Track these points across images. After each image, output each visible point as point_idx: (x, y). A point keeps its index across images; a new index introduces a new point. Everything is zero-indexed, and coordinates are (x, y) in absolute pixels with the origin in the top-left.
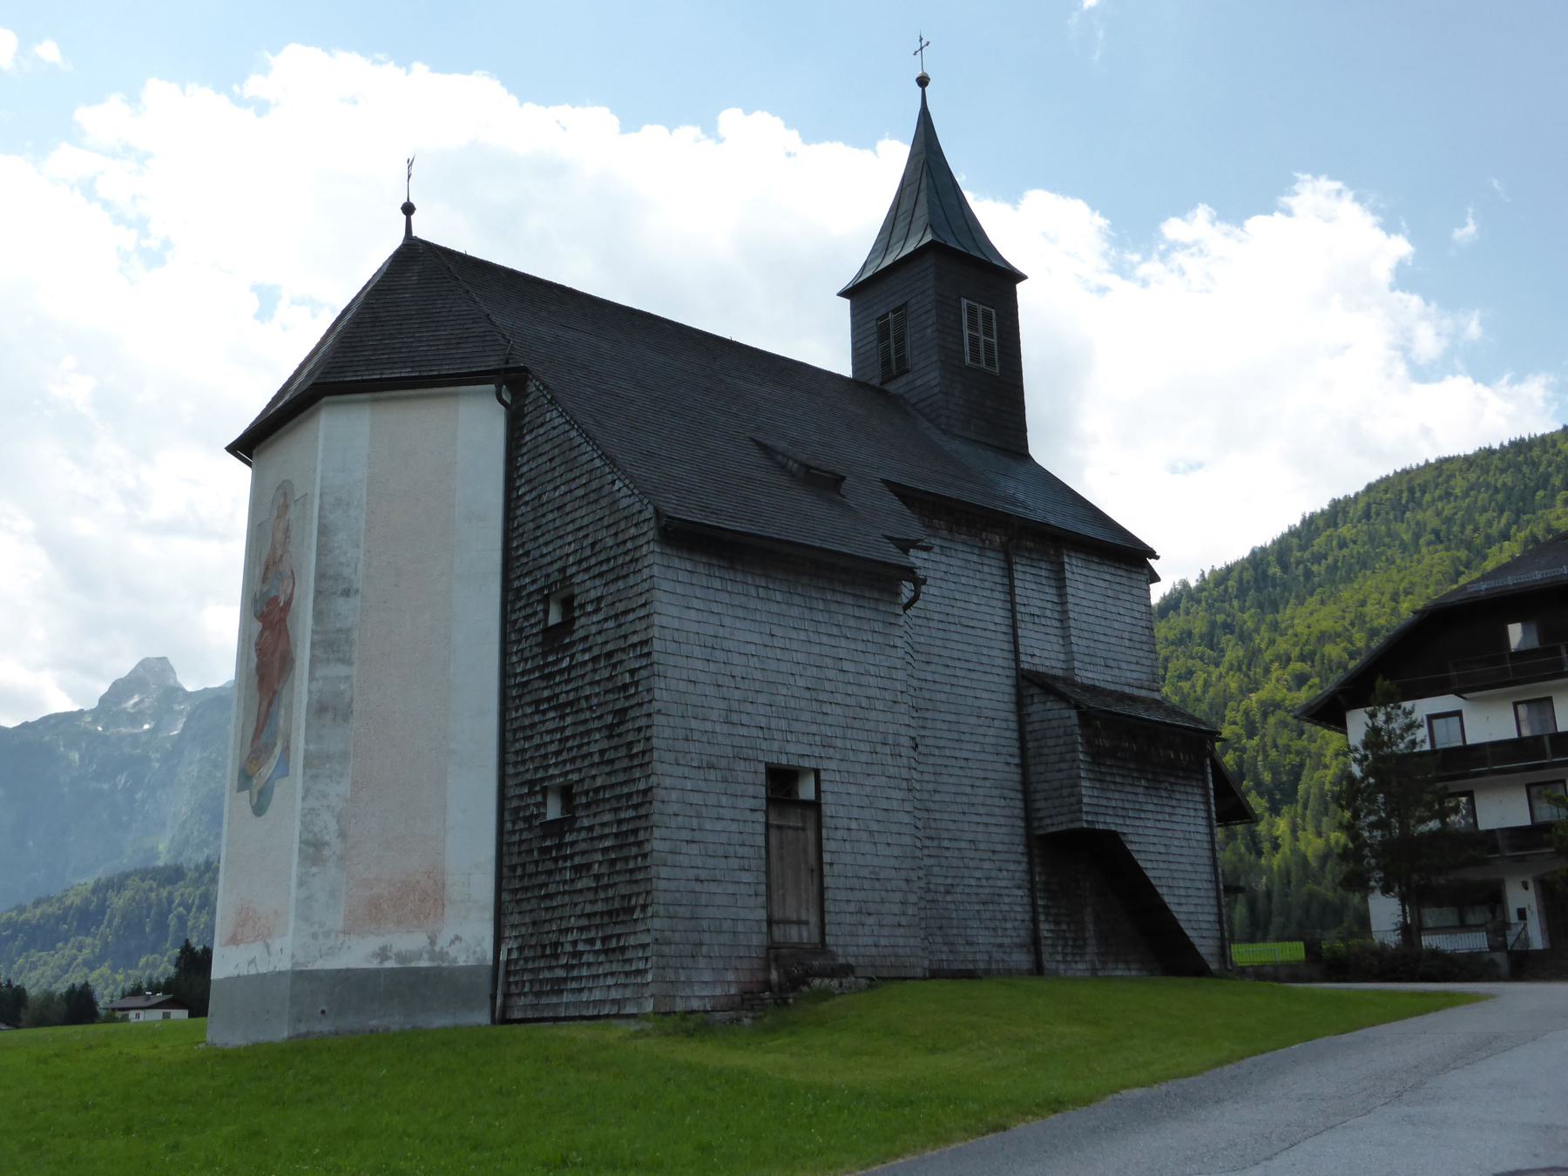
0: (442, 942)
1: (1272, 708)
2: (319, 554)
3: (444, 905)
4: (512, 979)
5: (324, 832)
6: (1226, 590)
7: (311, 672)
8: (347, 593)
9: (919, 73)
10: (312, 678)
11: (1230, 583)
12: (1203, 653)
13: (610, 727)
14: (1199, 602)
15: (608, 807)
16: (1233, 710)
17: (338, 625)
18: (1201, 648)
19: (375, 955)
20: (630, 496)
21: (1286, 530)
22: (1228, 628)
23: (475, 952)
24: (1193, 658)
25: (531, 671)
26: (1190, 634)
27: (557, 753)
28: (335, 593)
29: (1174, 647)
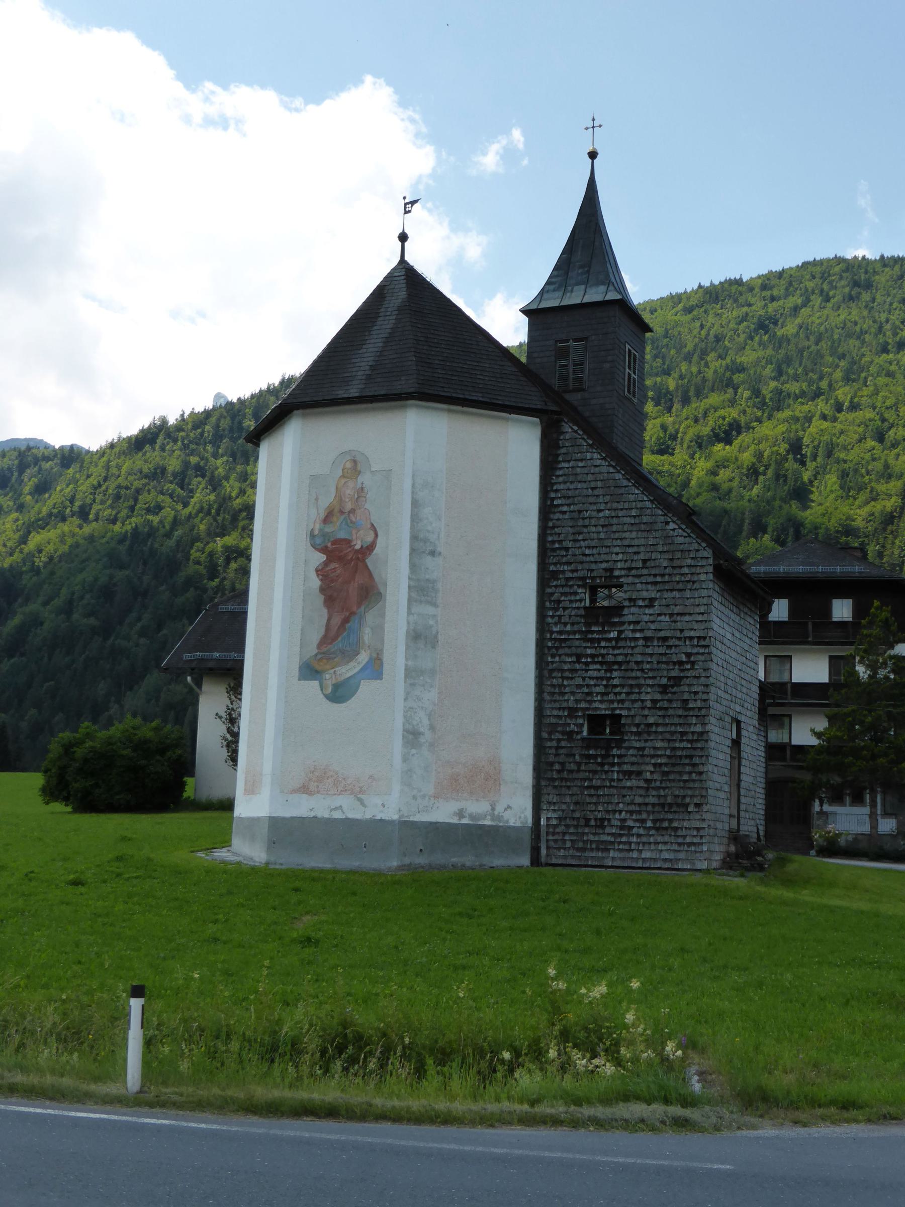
0: (499, 809)
1: (235, 555)
2: (413, 520)
3: (500, 784)
4: (551, 837)
5: (420, 725)
6: (202, 434)
7: (409, 608)
8: (433, 553)
9: (590, 149)
10: (409, 613)
11: (207, 428)
12: (174, 491)
13: (665, 687)
14: (175, 441)
15: (660, 737)
16: (199, 551)
17: (427, 577)
18: (172, 486)
19: (455, 814)
20: (685, 537)
21: (264, 387)
22: (200, 470)
23: (520, 817)
24: (163, 494)
25: (574, 633)
26: (163, 470)
27: (603, 694)
28: (424, 552)
29: (147, 481)
